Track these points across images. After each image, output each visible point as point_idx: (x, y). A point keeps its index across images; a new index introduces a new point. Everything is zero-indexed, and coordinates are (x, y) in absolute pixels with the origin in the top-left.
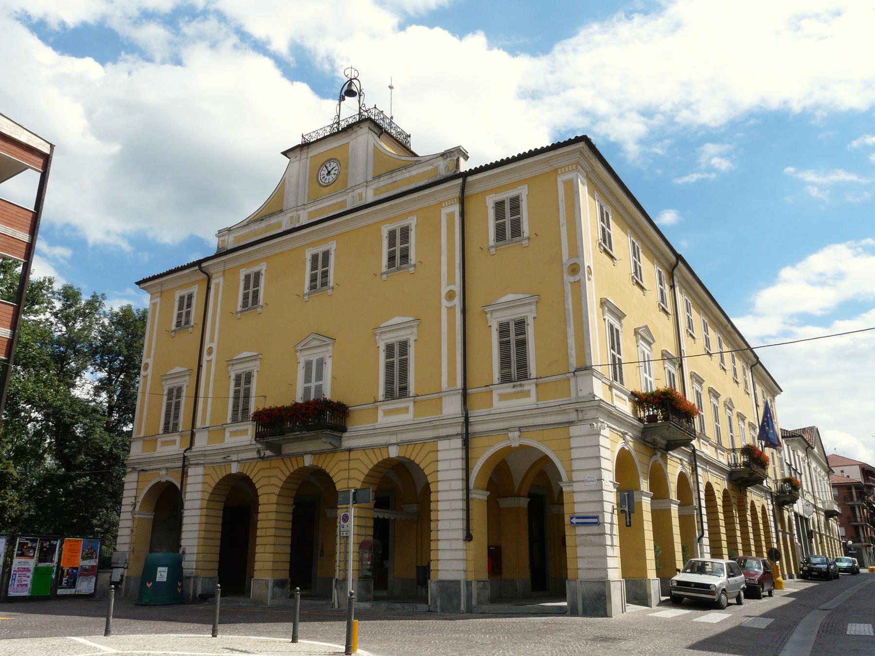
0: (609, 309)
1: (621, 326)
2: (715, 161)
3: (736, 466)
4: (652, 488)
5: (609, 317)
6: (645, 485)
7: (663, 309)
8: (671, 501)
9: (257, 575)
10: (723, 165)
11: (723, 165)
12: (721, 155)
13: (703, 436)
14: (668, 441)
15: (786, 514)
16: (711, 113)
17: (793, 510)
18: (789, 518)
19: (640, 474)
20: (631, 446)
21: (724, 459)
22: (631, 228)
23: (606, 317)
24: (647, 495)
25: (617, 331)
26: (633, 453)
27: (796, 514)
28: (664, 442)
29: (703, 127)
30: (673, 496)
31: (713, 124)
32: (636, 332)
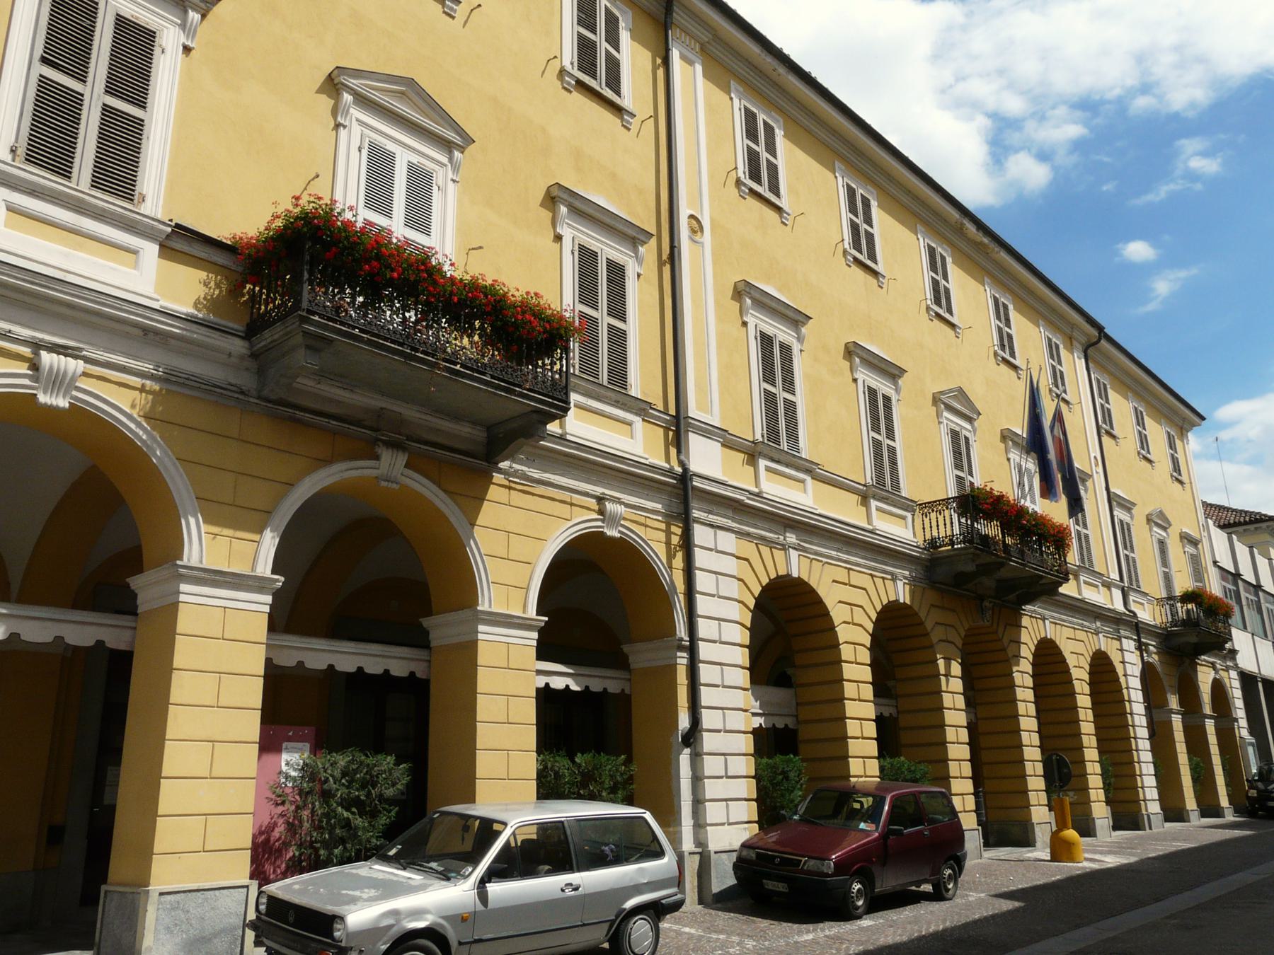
0: (863, 360)
1: (1132, 518)
2: (1197, 163)
3: (952, 543)
4: (1181, 704)
5: (867, 377)
6: (1174, 702)
7: (1177, 480)
8: (1171, 711)
9: (166, 874)
10: (1208, 166)
11: (1208, 166)
12: (1205, 154)
13: (1087, 566)
14: (489, 428)
15: (1205, 677)
16: (1186, 93)
17: (1236, 667)
18: (1219, 688)
19: (1167, 688)
20: (1154, 659)
21: (901, 531)
22: (1166, 417)
23: (1011, 456)
24: (1211, 717)
25: (1128, 525)
26: (1159, 668)
27: (1248, 680)
28: (480, 434)
29: (1175, 117)
30: (1207, 710)
31: (1191, 114)
32: (936, 400)
